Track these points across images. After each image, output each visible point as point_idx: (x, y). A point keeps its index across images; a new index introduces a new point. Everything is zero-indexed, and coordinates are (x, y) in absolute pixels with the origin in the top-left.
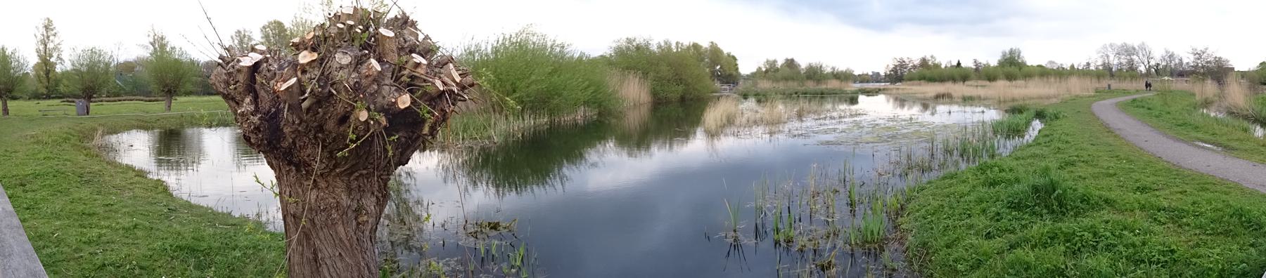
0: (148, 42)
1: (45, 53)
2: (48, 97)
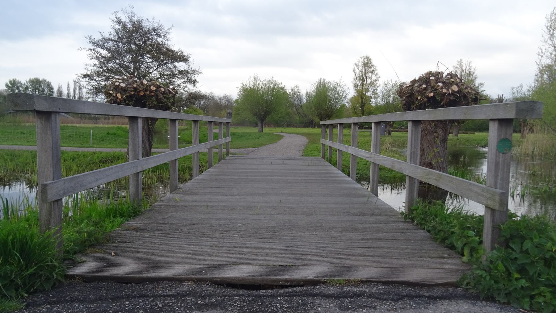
1: (362, 88)
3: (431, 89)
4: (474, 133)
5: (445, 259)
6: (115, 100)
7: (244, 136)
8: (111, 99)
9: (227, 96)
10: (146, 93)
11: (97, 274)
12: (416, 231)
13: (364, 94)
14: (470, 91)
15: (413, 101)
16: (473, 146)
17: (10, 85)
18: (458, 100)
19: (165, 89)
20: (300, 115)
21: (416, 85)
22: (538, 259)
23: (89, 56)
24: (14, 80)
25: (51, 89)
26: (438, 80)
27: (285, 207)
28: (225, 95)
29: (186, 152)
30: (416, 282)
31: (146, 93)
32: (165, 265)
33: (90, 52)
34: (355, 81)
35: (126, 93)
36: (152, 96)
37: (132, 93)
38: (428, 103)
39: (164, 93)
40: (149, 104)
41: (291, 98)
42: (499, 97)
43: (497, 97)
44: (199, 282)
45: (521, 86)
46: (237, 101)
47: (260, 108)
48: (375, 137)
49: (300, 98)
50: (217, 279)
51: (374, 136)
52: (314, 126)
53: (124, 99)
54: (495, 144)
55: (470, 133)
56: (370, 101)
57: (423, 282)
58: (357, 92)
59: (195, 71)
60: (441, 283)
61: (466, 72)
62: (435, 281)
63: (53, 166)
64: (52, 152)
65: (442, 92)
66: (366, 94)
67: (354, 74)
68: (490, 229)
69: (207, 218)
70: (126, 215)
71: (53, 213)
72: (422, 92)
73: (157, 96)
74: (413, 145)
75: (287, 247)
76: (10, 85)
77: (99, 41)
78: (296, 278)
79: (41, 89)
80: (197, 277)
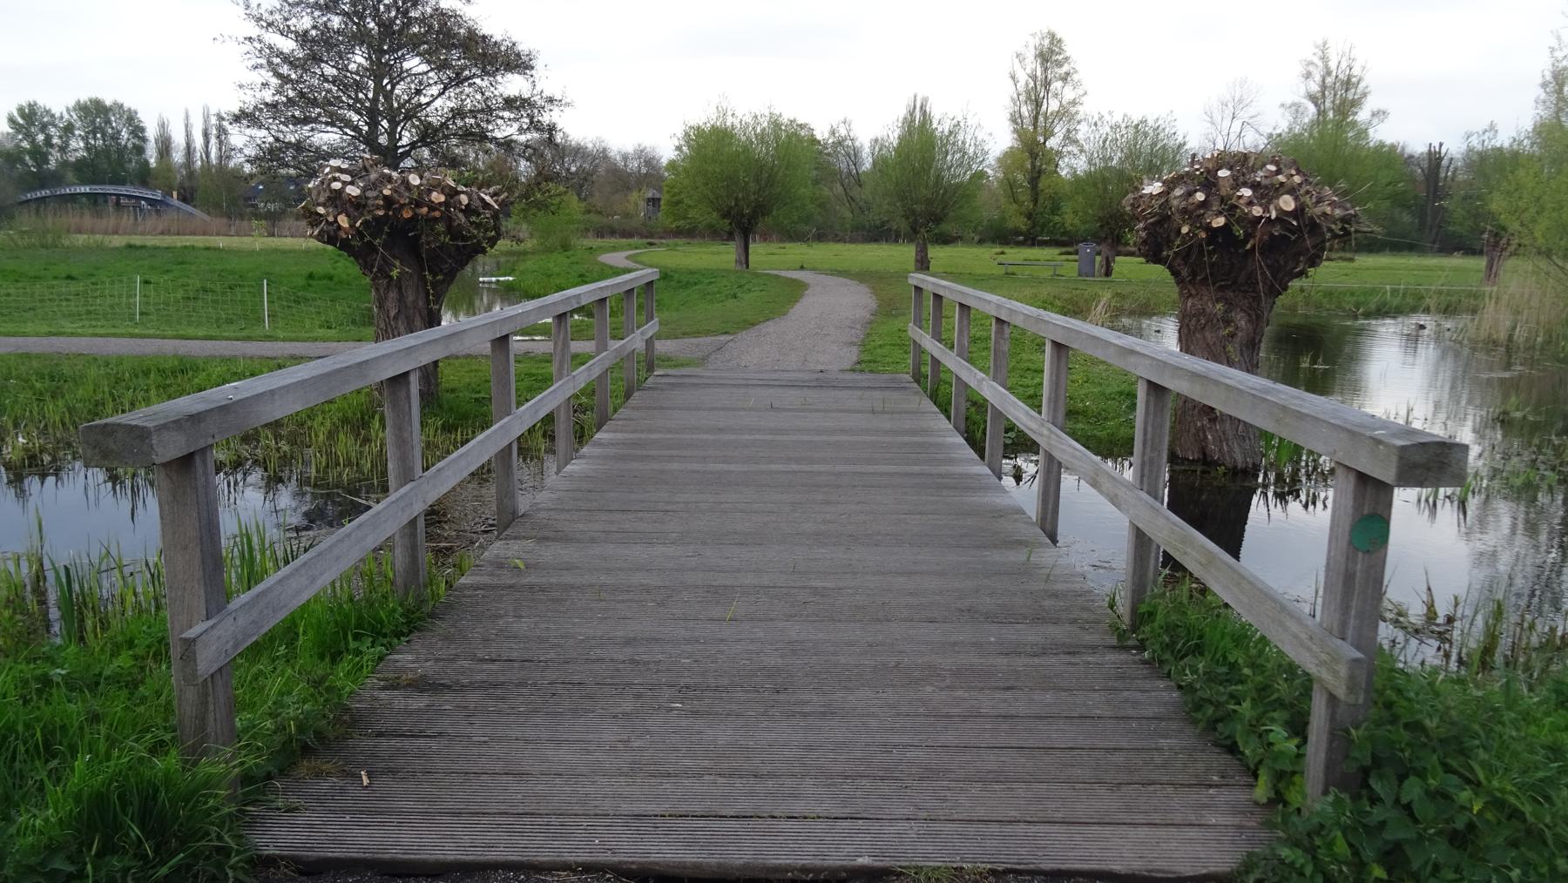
0: (1303, 92)
1: (1035, 125)
2: (1031, 240)
3: (1218, 203)
4: (1351, 260)
5: (1211, 791)
6: (332, 233)
7: (695, 284)
8: (322, 230)
9: (645, 148)
10: (417, 210)
11: (330, 854)
12: (1148, 685)
13: (1038, 144)
14: (1328, 210)
15: (1169, 236)
16: (1344, 311)
17: (21, 121)
18: (1293, 238)
19: (470, 199)
20: (853, 205)
21: (1178, 192)
22: (1435, 834)
23: (245, 57)
24: (30, 105)
25: (138, 131)
26: (1241, 179)
27: (804, 588)
28: (639, 146)
29: (536, 412)
30: (1130, 872)
31: (417, 210)
32: (499, 819)
33: (248, 46)
34: (1015, 104)
35: (362, 215)
36: (435, 220)
37: (381, 213)
38: (1208, 245)
39: (469, 211)
40: (428, 243)
41: (829, 154)
42: (1430, 150)
43: (1425, 149)
44: (587, 873)
45: (1492, 128)
46: (672, 165)
47: (740, 195)
48: (1054, 378)
49: (854, 155)
50: (629, 866)
51: (1051, 374)
52: (893, 237)
53: (358, 229)
54: (1347, 529)
55: (1341, 258)
56: (1057, 166)
57: (1146, 873)
58: (1019, 136)
59: (551, 100)
60: (1192, 874)
61: (1337, 77)
62: (1177, 868)
63: (205, 584)
64: (201, 550)
65: (1250, 216)
66: (1045, 143)
67: (1011, 82)
68: (1325, 737)
69: (601, 638)
70: (388, 631)
71: (210, 699)
72: (1194, 214)
73: (449, 220)
74: (1149, 443)
75: (810, 748)
76: (21, 121)
77: (271, 13)
78: (826, 863)
79: (110, 131)
80: (579, 859)
